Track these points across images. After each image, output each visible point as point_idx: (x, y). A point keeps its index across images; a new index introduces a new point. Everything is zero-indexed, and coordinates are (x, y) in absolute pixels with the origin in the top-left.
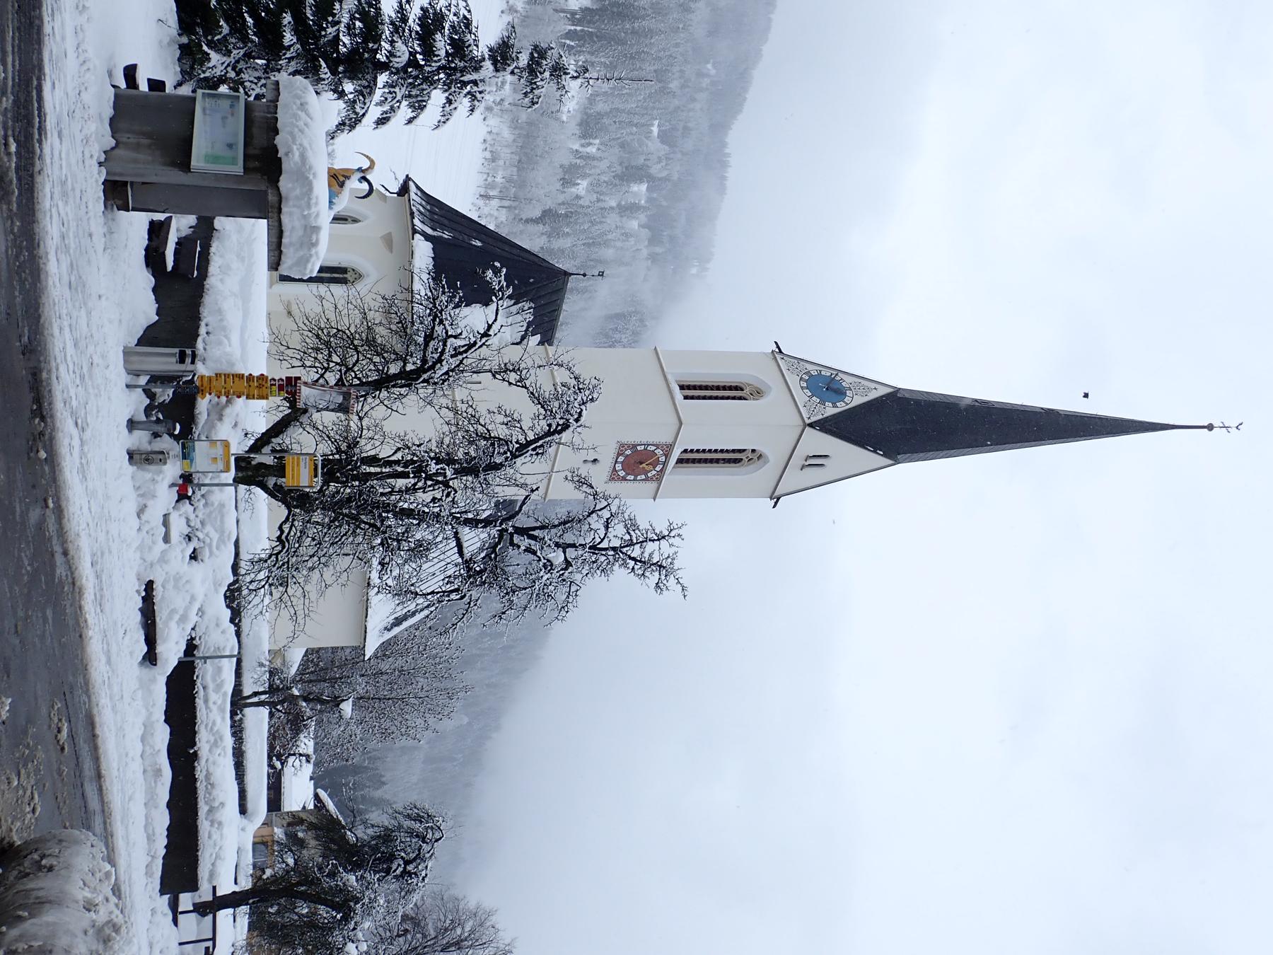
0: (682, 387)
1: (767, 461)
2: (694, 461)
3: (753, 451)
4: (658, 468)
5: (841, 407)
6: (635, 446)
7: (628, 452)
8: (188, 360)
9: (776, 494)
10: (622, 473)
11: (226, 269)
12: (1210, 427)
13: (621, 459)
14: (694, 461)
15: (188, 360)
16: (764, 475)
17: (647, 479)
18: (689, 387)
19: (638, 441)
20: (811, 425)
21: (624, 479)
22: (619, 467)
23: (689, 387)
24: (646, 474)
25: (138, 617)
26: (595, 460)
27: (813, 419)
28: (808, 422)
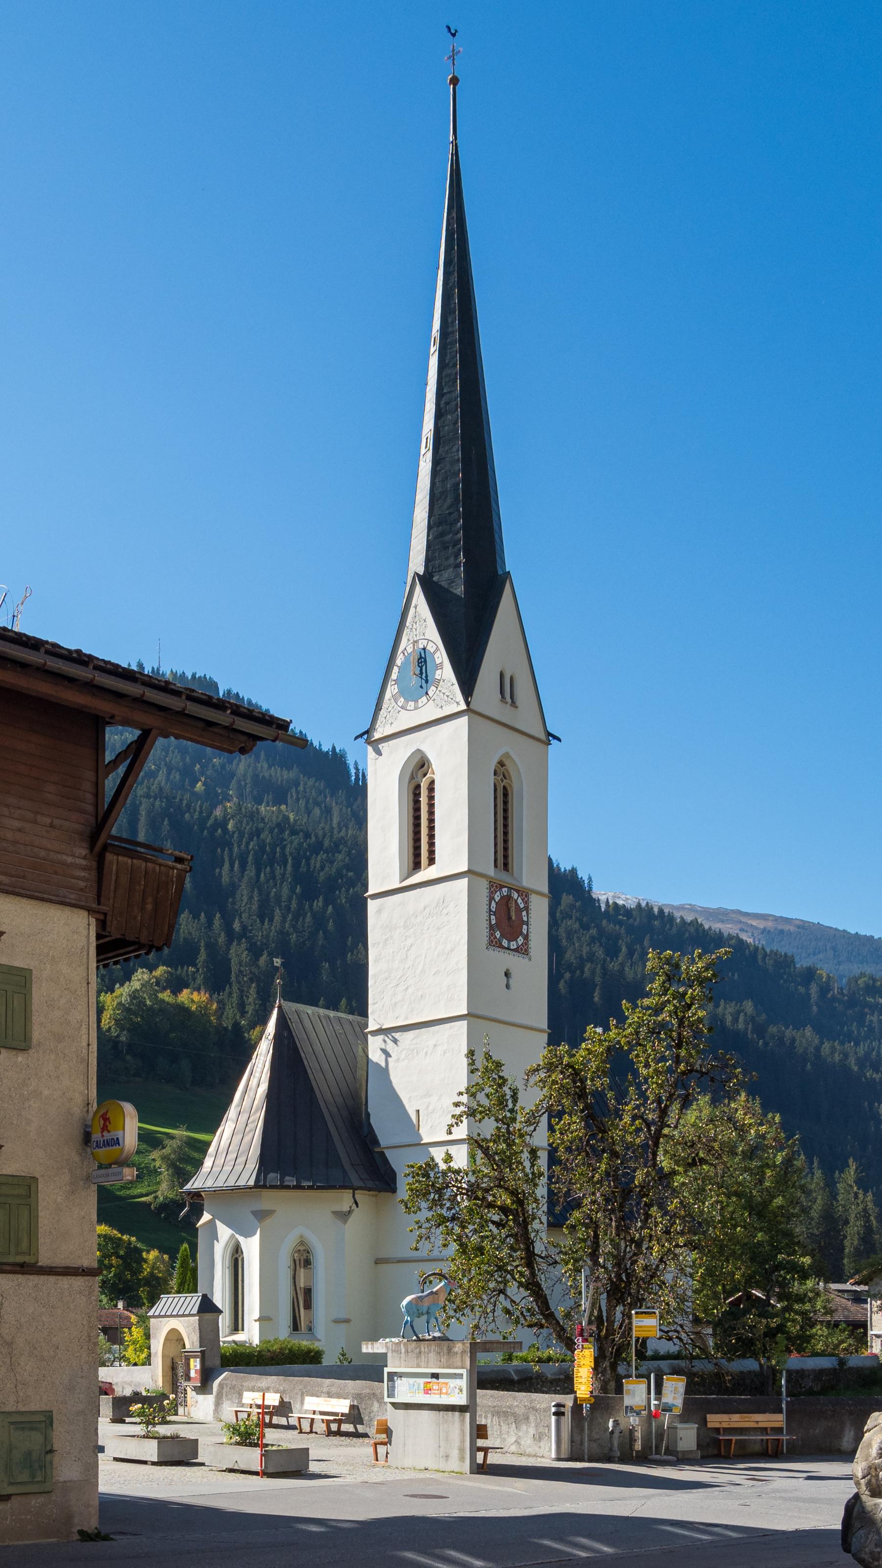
0: (417, 865)
1: (507, 755)
2: (506, 857)
3: (495, 774)
4: (515, 895)
5: (441, 657)
6: (491, 927)
7: (498, 934)
8: (562, 1409)
9: (543, 736)
10: (520, 940)
11: (515, 1398)
12: (455, 81)
13: (505, 943)
14: (506, 857)
15: (562, 1409)
16: (520, 753)
17: (527, 908)
18: (417, 854)
19: (485, 924)
20: (468, 704)
21: (526, 938)
22: (513, 945)
23: (417, 854)
24: (521, 910)
25: (400, 614)
26: (507, 974)
27: (459, 697)
28: (463, 707)
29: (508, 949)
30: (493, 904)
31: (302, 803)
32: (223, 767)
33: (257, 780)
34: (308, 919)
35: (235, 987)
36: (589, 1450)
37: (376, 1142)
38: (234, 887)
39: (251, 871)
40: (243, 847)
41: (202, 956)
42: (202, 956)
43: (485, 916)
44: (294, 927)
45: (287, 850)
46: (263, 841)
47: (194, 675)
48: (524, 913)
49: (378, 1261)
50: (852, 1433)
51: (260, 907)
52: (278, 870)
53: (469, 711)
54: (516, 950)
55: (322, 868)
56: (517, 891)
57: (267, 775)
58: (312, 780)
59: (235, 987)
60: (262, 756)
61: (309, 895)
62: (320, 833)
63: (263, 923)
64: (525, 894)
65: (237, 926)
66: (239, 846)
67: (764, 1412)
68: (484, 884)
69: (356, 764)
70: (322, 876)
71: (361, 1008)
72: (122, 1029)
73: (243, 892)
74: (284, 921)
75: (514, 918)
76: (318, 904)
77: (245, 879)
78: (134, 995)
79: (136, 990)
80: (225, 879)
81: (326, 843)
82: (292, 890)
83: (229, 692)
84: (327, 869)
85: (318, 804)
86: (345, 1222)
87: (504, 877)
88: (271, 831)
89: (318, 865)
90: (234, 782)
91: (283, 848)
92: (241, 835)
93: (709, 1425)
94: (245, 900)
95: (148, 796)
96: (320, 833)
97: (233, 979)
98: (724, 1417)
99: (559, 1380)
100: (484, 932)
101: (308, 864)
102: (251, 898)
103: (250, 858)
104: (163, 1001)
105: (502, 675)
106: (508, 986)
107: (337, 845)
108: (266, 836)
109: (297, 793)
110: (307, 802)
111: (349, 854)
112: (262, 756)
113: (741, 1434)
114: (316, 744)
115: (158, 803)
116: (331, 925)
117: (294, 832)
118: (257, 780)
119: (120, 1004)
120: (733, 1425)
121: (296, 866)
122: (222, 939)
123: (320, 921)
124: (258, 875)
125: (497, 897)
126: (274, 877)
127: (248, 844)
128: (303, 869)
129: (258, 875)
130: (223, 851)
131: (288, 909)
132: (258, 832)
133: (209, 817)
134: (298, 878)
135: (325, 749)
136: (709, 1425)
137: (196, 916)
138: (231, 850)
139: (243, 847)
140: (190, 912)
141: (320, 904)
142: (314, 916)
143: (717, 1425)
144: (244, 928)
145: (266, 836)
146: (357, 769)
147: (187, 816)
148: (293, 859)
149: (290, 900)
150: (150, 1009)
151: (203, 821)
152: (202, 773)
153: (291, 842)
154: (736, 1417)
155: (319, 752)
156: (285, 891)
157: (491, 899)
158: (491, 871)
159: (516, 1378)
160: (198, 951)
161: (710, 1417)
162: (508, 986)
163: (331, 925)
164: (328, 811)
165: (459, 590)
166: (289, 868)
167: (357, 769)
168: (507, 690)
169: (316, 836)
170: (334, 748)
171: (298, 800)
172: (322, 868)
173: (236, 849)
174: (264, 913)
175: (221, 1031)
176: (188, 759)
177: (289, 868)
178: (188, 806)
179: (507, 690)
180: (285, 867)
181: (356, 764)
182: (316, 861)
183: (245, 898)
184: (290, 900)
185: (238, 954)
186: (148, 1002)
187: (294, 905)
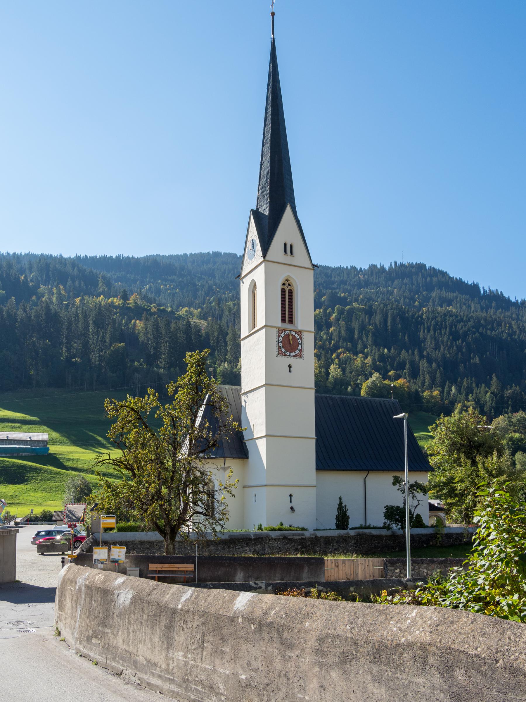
4: (294, 333)
7: (283, 350)
12: (273, 14)
13: (288, 353)
21: (301, 350)
29: (290, 356)
30: (281, 338)
31: (458, 304)
32: (427, 295)
33: (440, 298)
34: (455, 348)
35: (421, 376)
36: (404, 563)
37: (244, 439)
38: (425, 339)
39: (432, 332)
40: (429, 324)
41: (408, 365)
42: (408, 365)
43: (276, 343)
44: (449, 352)
45: (447, 323)
46: (437, 321)
47: (416, 263)
48: (299, 340)
49: (244, 487)
50: (242, 574)
51: (435, 345)
52: (443, 331)
53: (264, 260)
54: (295, 356)
55: (462, 328)
56: (295, 332)
57: (444, 296)
58: (464, 296)
59: (421, 376)
60: (443, 289)
61: (455, 339)
62: (462, 315)
63: (436, 351)
64: (300, 333)
65: (425, 353)
66: (427, 324)
67: (183, 563)
68: (275, 332)
69: (483, 287)
70: (461, 331)
71: (240, 385)
72: (369, 395)
73: (428, 340)
74: (444, 350)
75: (291, 343)
76: (459, 342)
77: (429, 336)
78: (373, 382)
79: (374, 381)
80: (421, 336)
81: (465, 319)
82: (449, 338)
83: (430, 267)
84: (463, 329)
85: (465, 304)
86: (225, 471)
87: (287, 326)
88: (441, 317)
89: (460, 327)
90: (431, 301)
91: (445, 323)
92: (428, 320)
93: (150, 569)
94: (429, 343)
95: (391, 309)
96: (462, 315)
97: (421, 373)
98: (159, 565)
99: (280, 538)
100: (275, 350)
101: (456, 327)
102: (431, 343)
103: (432, 327)
104: (385, 384)
105: (285, 245)
106: (290, 371)
107: (469, 319)
108: (439, 319)
109: (456, 301)
110: (460, 304)
111: (474, 322)
112: (443, 289)
113: (172, 574)
114: (466, 282)
115: (395, 311)
116: (464, 350)
117: (451, 316)
118: (440, 298)
119: (368, 386)
120: (163, 569)
121: (451, 329)
122: (417, 358)
123: (459, 349)
124: (435, 334)
125: (283, 335)
126: (441, 334)
127: (431, 323)
128: (454, 329)
129: (435, 334)
130: (421, 326)
131: (447, 345)
132: (436, 317)
133: (415, 314)
134: (451, 333)
135: (470, 283)
136: (150, 569)
137: (407, 351)
138: (424, 325)
139: (429, 324)
140: (405, 350)
141: (460, 342)
142: (457, 347)
143: (155, 569)
144: (428, 354)
145: (439, 319)
146: (484, 289)
147: (407, 315)
148: (450, 326)
149: (447, 341)
150: (379, 387)
151: (413, 316)
152: (418, 298)
153: (449, 320)
154: (166, 565)
155: (467, 285)
156: (445, 339)
157: (279, 336)
158: (279, 324)
159: (253, 537)
160: (406, 364)
161: (150, 565)
162: (290, 371)
163: (464, 350)
164: (469, 306)
165: (267, 213)
166: (448, 330)
167: (484, 289)
168: (289, 250)
169: (461, 317)
170: (474, 283)
171: (457, 304)
172: (462, 328)
173: (426, 325)
174: (437, 347)
175: (409, 394)
176: (412, 294)
177: (448, 330)
178: (408, 311)
179: (289, 250)
180: (446, 330)
181: (483, 287)
182: (459, 326)
183: (429, 343)
184: (447, 341)
185: (423, 364)
186: (379, 385)
187: (449, 343)
